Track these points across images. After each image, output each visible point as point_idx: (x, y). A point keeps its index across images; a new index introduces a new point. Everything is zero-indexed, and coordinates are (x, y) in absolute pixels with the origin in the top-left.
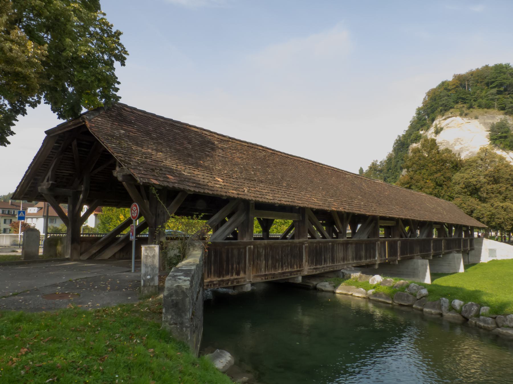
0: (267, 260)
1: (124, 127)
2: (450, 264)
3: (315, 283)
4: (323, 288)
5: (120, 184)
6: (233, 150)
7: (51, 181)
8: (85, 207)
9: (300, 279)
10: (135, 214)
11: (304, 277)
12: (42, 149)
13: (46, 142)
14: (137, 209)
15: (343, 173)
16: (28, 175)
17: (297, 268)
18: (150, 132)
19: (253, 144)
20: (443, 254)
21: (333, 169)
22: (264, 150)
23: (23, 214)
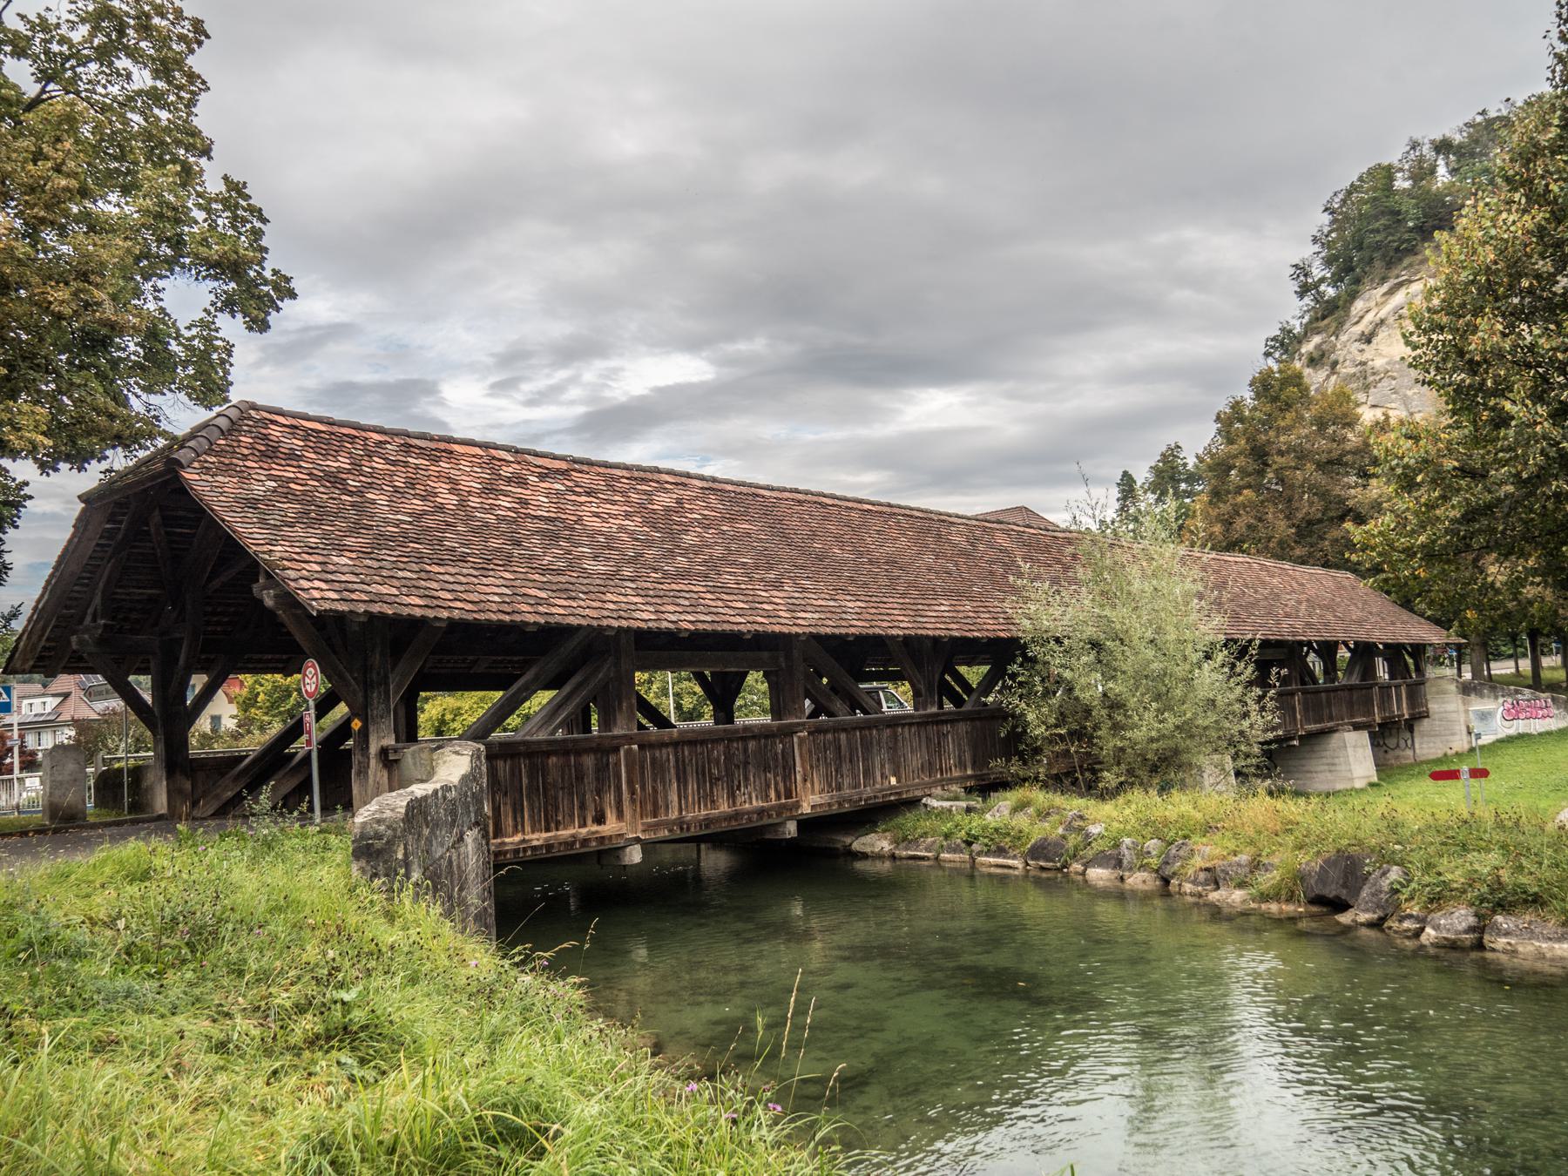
0: (682, 780)
1: (273, 472)
2: (1333, 764)
3: (848, 840)
4: (868, 850)
5: (270, 613)
6: (579, 494)
7: (102, 618)
8: (198, 681)
9: (791, 829)
10: (314, 686)
11: (806, 824)
12: (76, 540)
13: (82, 523)
14: (316, 674)
15: (943, 521)
16: (43, 608)
17: (778, 797)
18: (344, 476)
19: (644, 470)
20: (1301, 737)
21: (908, 512)
22: (682, 484)
23: (5, 696)
